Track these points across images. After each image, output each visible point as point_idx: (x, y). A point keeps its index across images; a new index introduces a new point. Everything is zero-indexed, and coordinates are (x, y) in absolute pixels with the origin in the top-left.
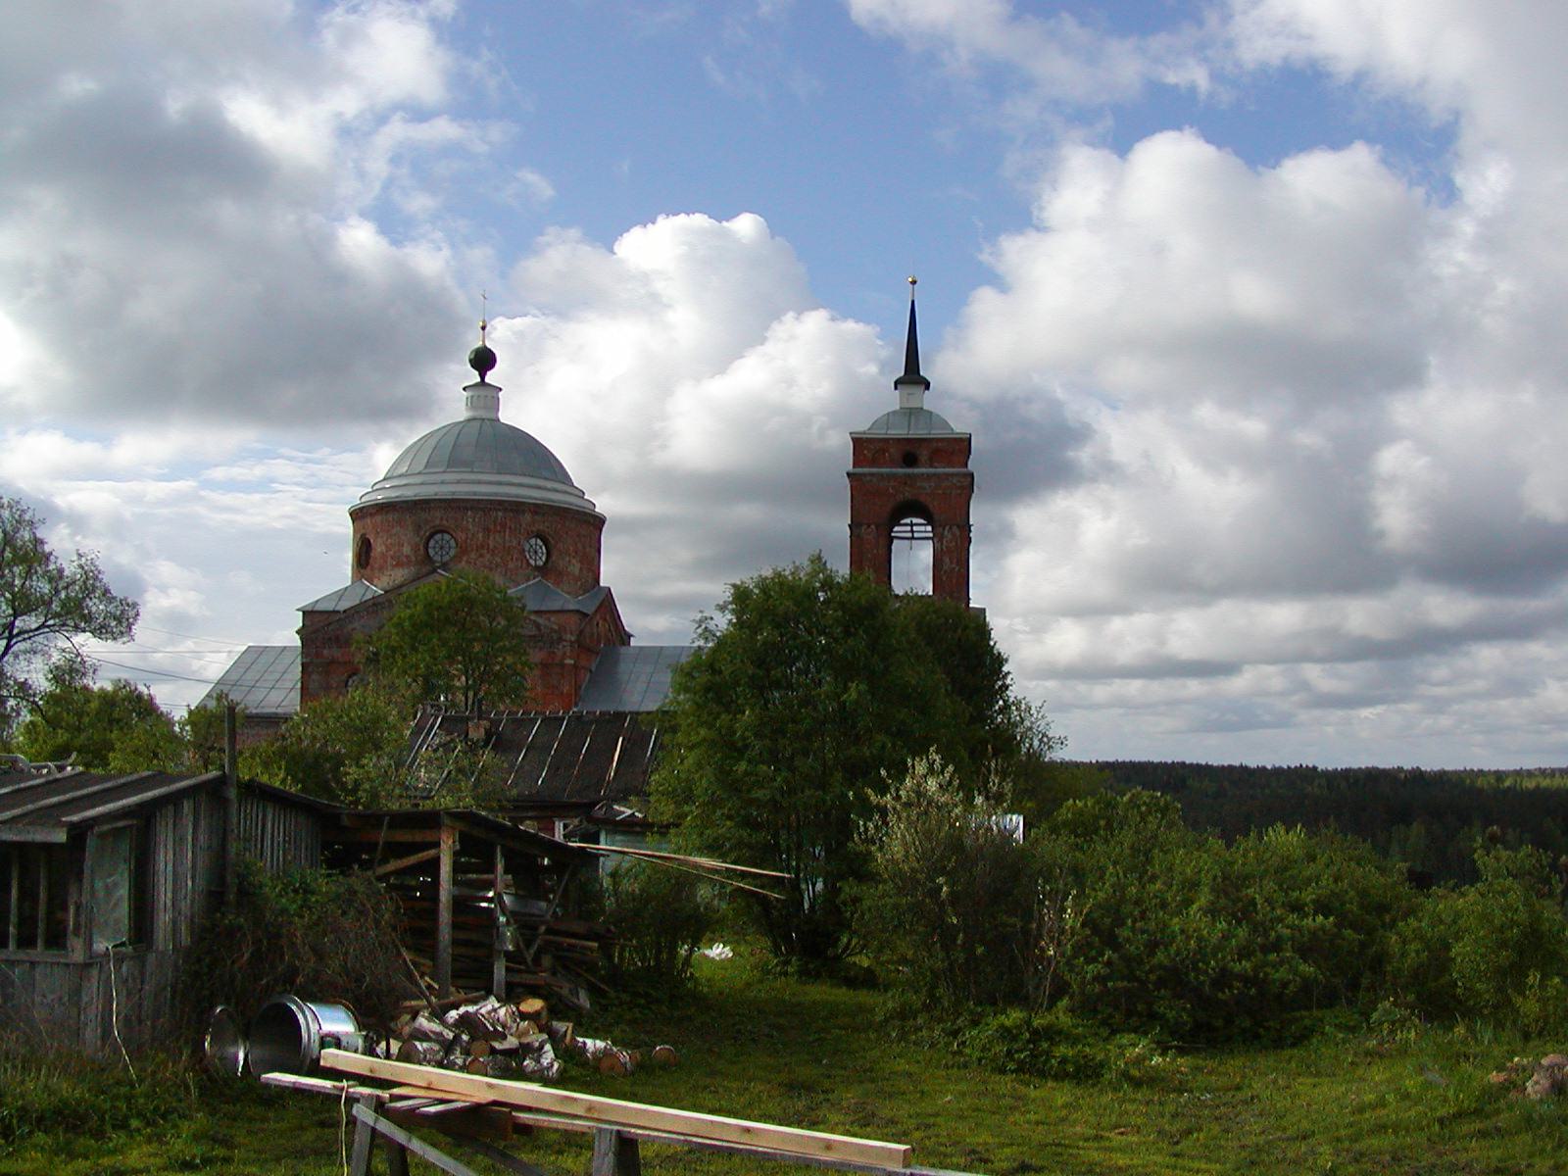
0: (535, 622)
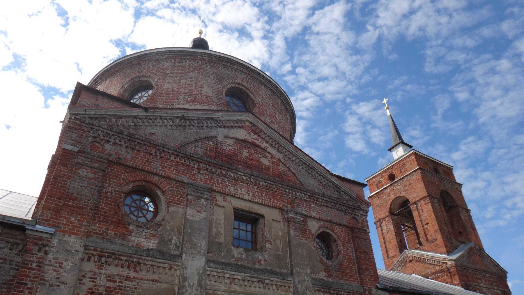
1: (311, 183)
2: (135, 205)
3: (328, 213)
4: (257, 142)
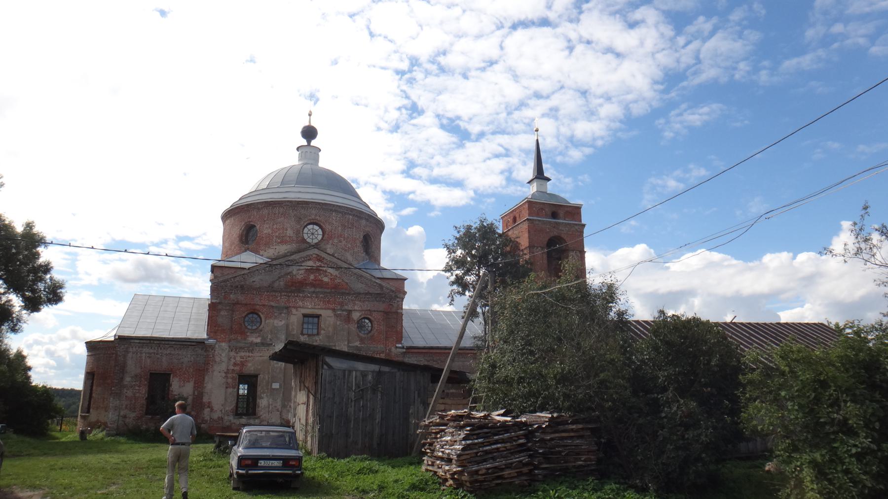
0: (380, 284)
2: (314, 232)
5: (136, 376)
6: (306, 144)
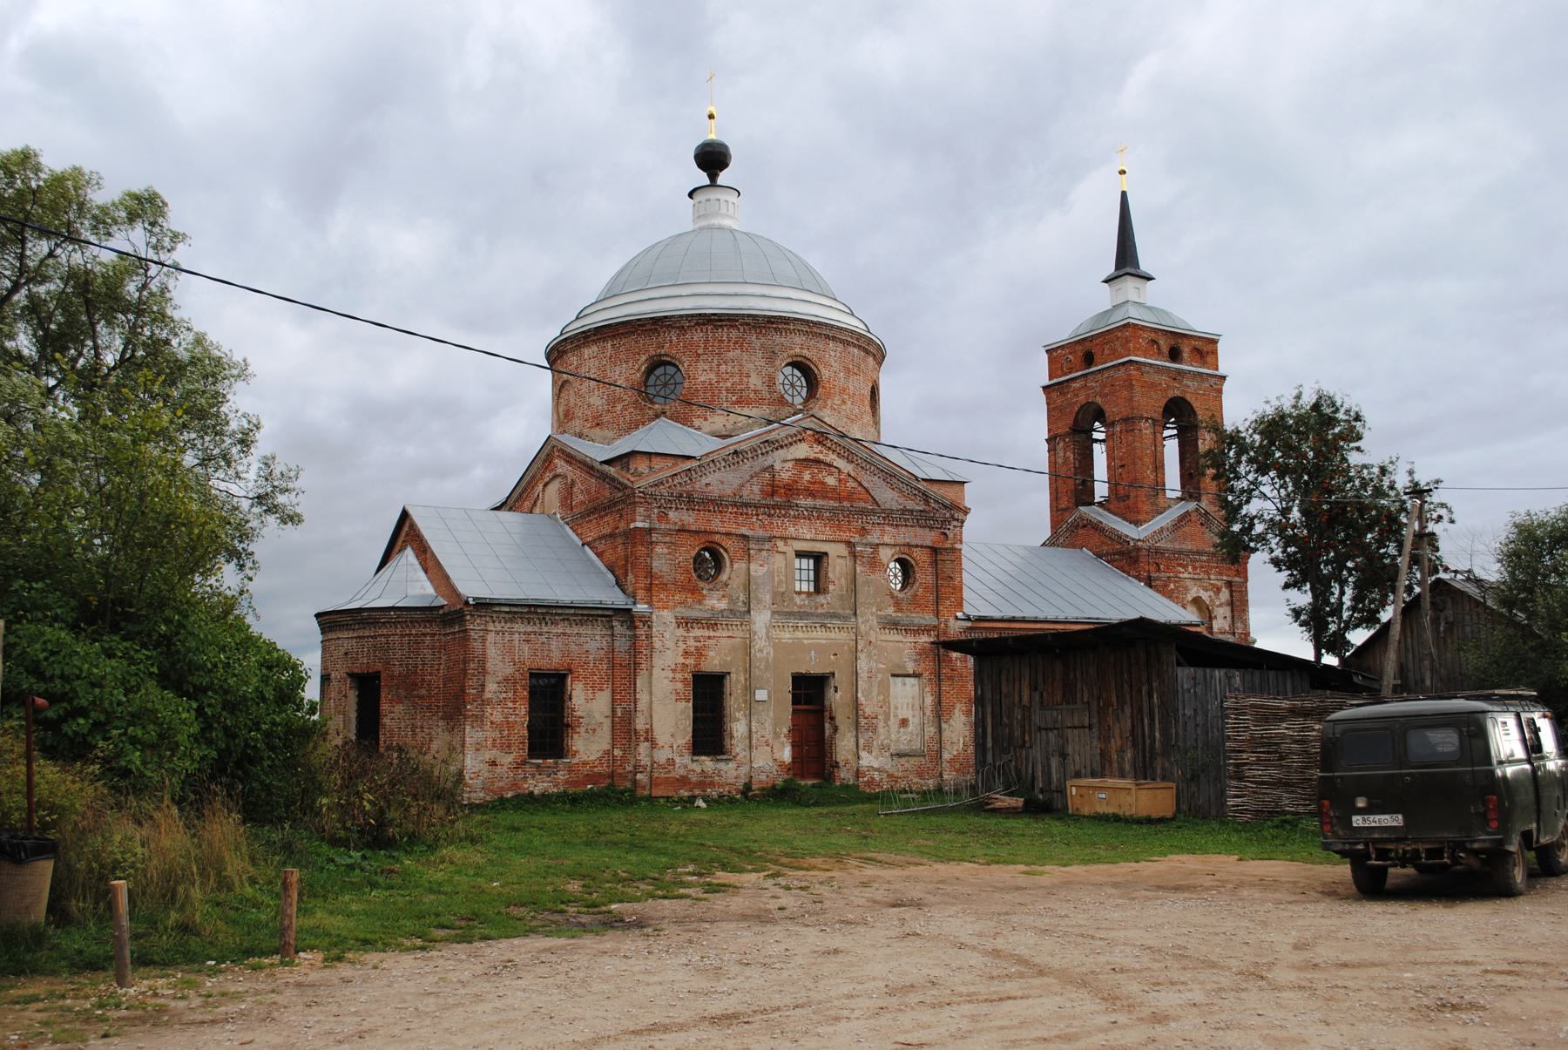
1: (888, 497)
3: (907, 535)
4: (821, 457)
5: (506, 680)
6: (708, 182)
